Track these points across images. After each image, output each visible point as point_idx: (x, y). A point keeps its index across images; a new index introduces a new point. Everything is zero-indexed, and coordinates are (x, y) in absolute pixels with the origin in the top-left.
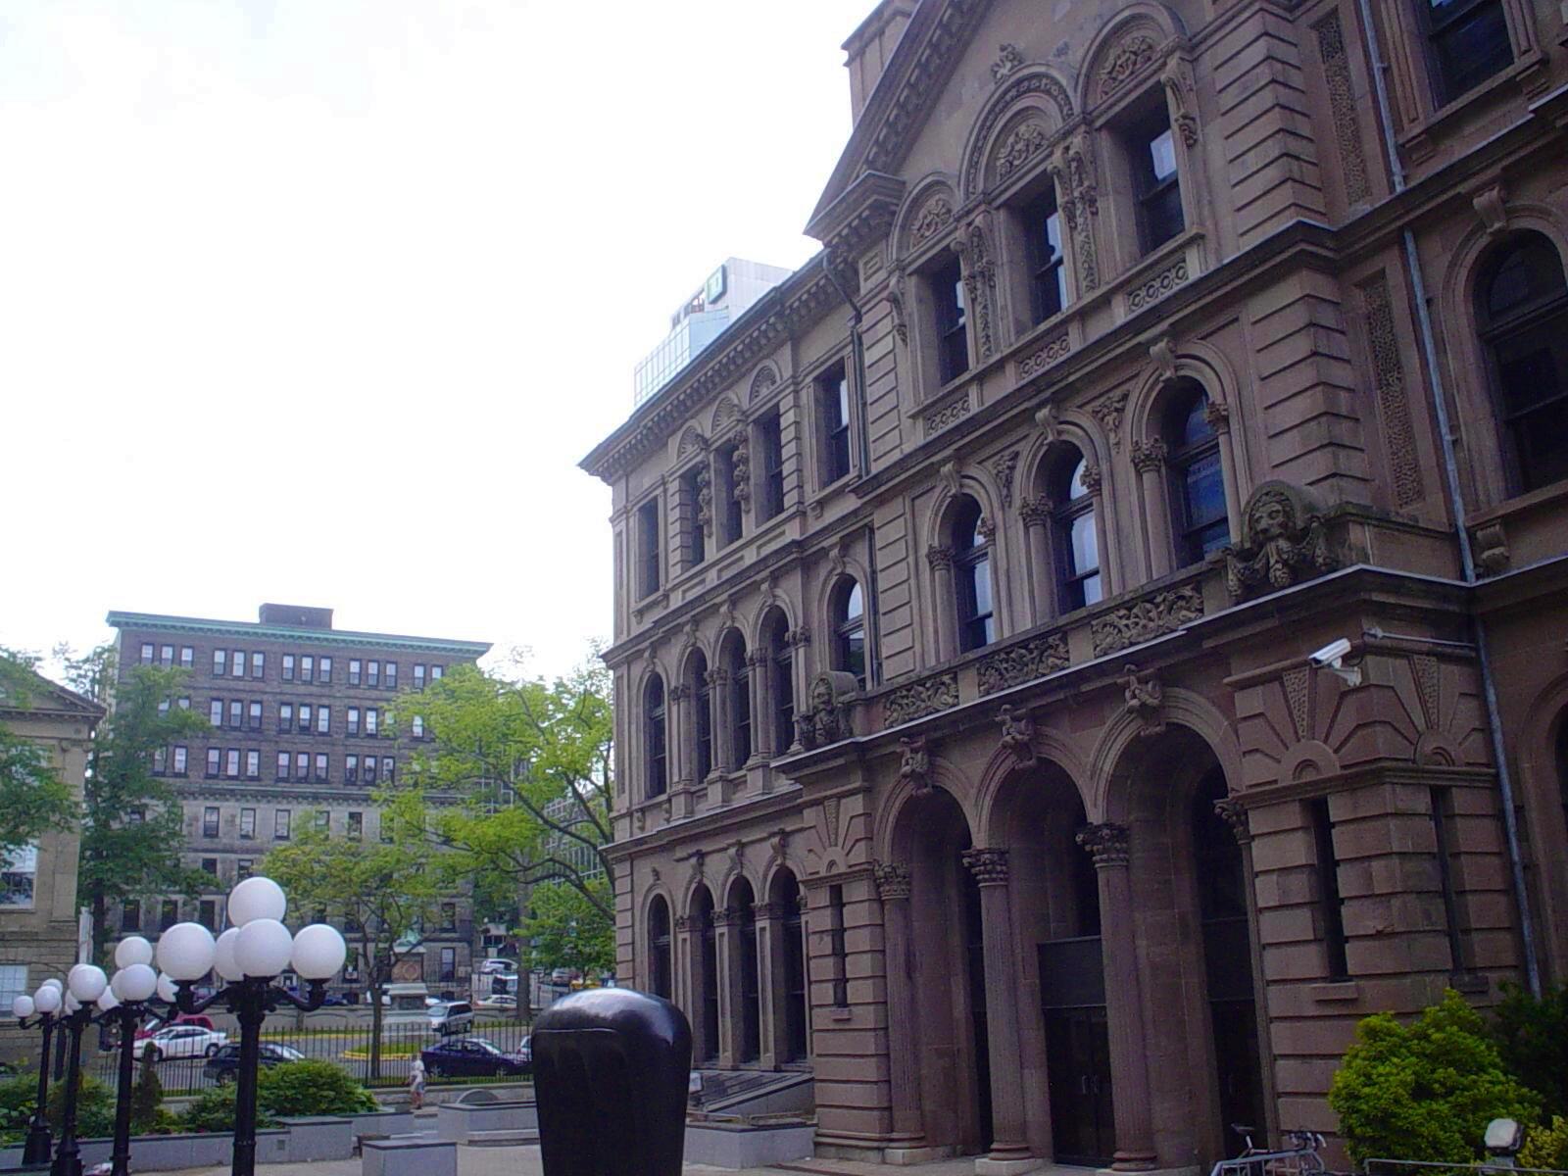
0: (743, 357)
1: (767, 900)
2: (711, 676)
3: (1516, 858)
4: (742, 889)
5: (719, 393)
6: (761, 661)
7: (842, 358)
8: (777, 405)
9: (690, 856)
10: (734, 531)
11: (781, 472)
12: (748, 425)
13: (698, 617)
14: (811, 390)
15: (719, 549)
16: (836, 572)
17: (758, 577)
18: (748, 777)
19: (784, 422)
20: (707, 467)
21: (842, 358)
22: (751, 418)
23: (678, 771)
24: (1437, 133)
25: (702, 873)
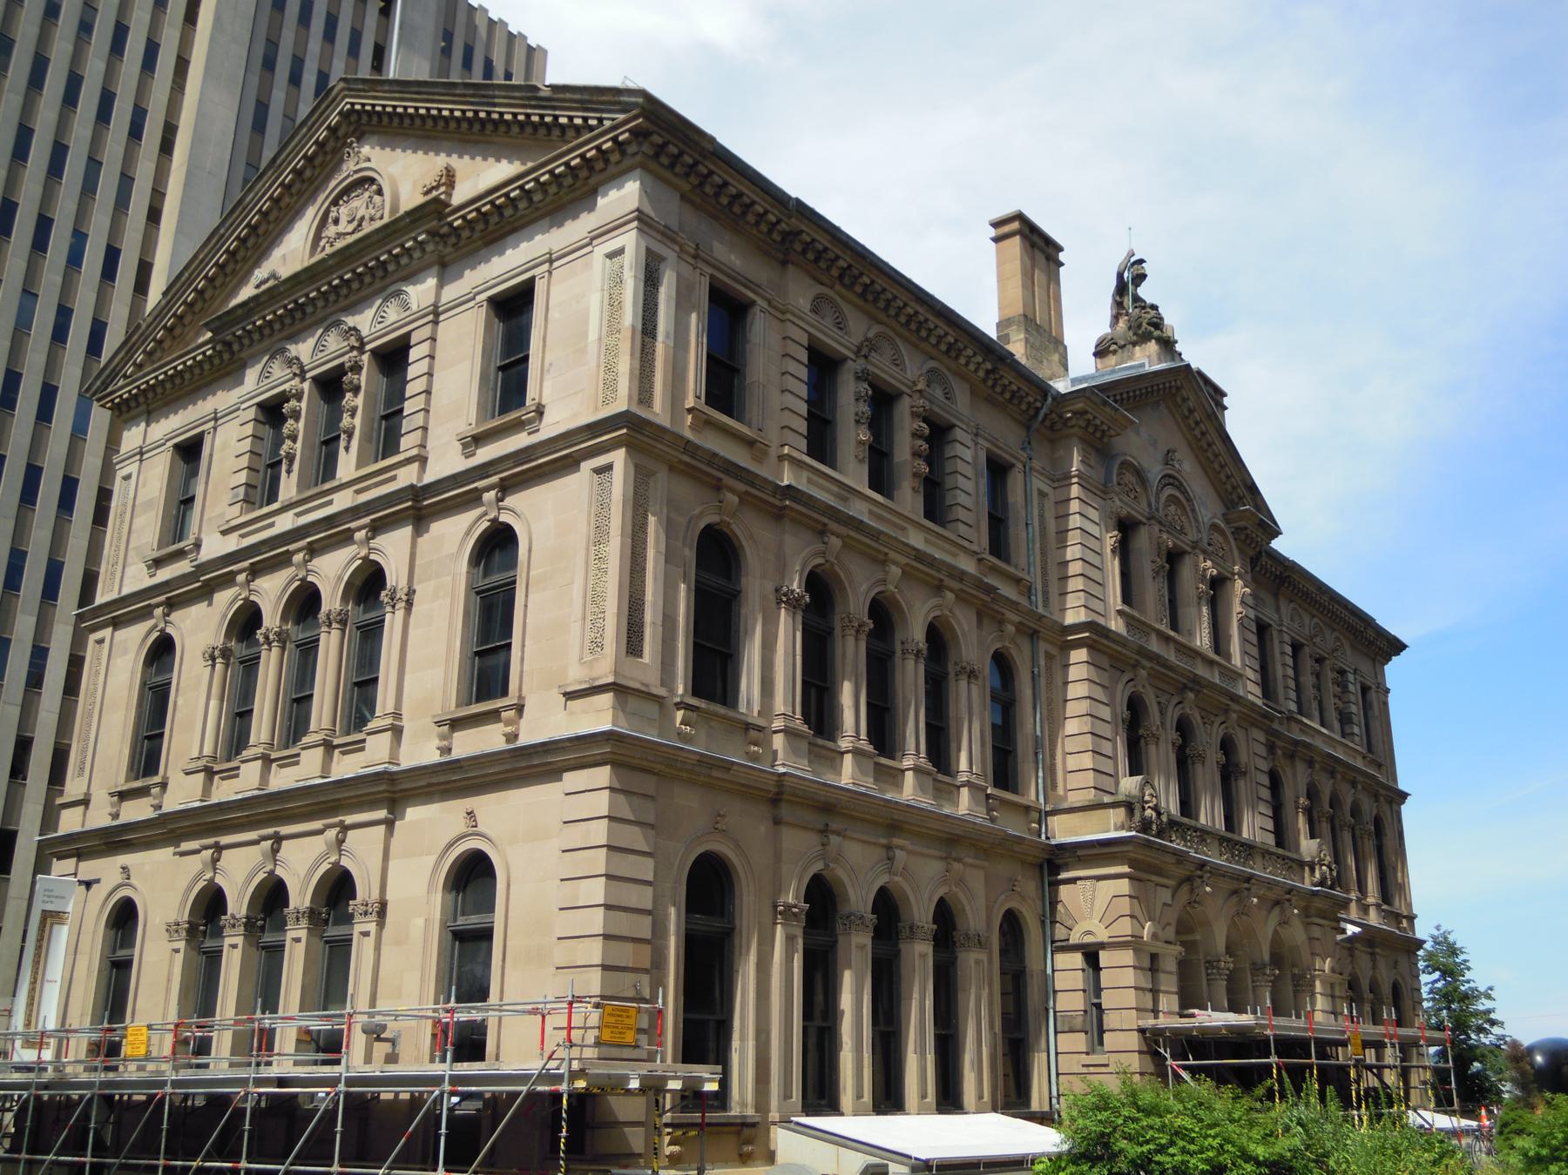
0: (398, 263)
1: (307, 903)
2: (267, 638)
3: (245, 1017)
4: (272, 896)
5: (332, 314)
6: (340, 622)
7: (203, 432)
8: (408, 335)
9: (265, 838)
10: (328, 467)
11: (401, 410)
12: (364, 353)
13: (257, 567)
14: (170, 453)
15: (359, 466)
16: (487, 517)
17: (153, 601)
18: (367, 745)
19: (414, 354)
20: (299, 396)
21: (532, 280)
22: (368, 347)
23: (261, 728)
24: (478, 440)
25: (215, 869)
